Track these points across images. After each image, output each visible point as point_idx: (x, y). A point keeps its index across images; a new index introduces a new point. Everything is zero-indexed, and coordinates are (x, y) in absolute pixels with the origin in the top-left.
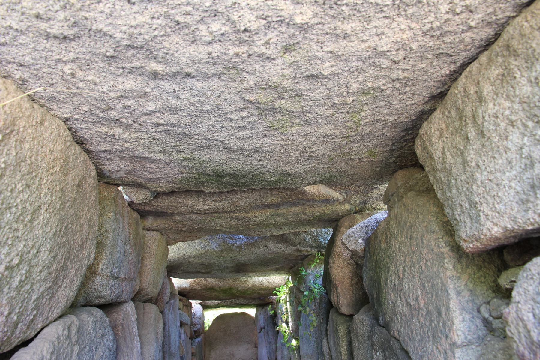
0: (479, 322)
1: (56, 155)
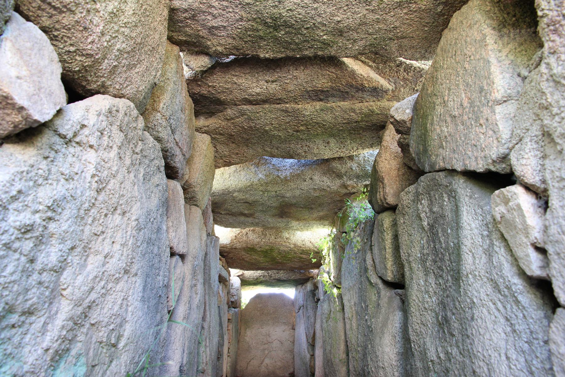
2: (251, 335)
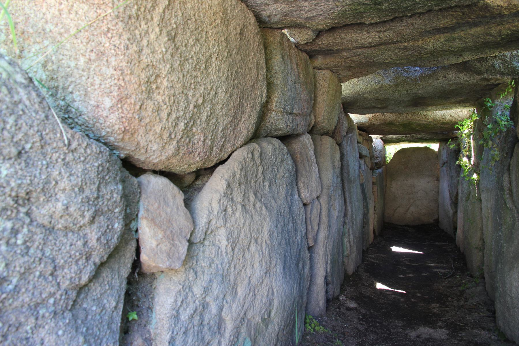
1: (215, 10)
2: (396, 187)
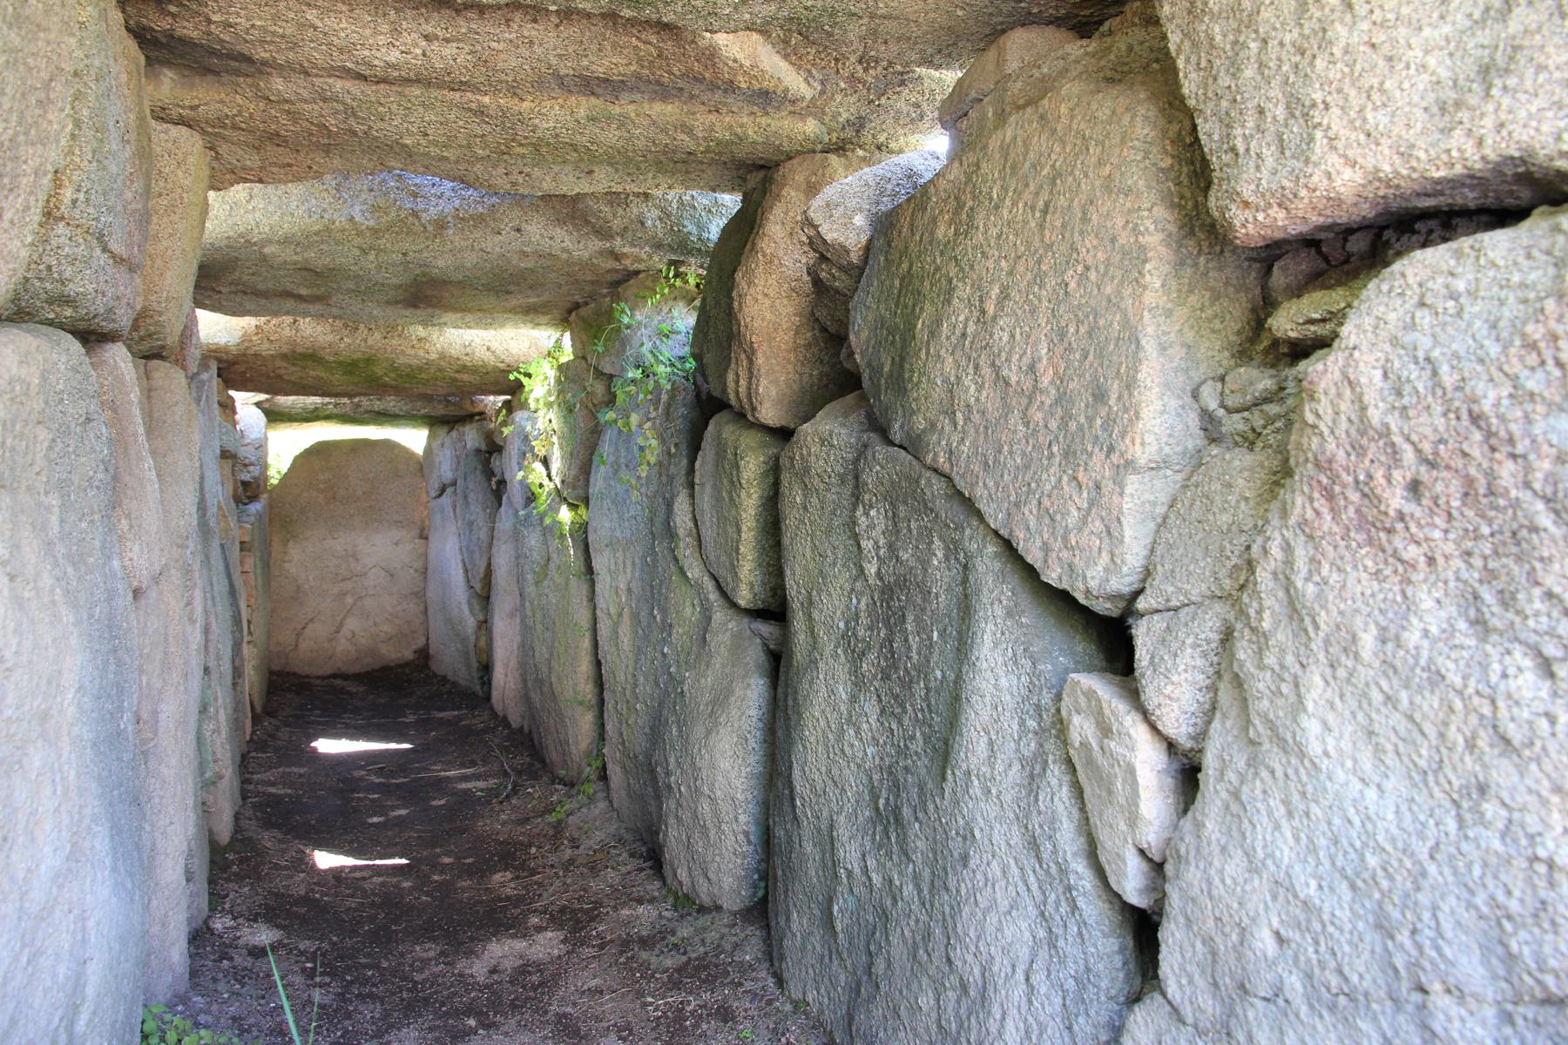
0: (1193, 419)
2: (302, 559)
